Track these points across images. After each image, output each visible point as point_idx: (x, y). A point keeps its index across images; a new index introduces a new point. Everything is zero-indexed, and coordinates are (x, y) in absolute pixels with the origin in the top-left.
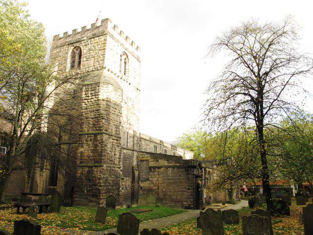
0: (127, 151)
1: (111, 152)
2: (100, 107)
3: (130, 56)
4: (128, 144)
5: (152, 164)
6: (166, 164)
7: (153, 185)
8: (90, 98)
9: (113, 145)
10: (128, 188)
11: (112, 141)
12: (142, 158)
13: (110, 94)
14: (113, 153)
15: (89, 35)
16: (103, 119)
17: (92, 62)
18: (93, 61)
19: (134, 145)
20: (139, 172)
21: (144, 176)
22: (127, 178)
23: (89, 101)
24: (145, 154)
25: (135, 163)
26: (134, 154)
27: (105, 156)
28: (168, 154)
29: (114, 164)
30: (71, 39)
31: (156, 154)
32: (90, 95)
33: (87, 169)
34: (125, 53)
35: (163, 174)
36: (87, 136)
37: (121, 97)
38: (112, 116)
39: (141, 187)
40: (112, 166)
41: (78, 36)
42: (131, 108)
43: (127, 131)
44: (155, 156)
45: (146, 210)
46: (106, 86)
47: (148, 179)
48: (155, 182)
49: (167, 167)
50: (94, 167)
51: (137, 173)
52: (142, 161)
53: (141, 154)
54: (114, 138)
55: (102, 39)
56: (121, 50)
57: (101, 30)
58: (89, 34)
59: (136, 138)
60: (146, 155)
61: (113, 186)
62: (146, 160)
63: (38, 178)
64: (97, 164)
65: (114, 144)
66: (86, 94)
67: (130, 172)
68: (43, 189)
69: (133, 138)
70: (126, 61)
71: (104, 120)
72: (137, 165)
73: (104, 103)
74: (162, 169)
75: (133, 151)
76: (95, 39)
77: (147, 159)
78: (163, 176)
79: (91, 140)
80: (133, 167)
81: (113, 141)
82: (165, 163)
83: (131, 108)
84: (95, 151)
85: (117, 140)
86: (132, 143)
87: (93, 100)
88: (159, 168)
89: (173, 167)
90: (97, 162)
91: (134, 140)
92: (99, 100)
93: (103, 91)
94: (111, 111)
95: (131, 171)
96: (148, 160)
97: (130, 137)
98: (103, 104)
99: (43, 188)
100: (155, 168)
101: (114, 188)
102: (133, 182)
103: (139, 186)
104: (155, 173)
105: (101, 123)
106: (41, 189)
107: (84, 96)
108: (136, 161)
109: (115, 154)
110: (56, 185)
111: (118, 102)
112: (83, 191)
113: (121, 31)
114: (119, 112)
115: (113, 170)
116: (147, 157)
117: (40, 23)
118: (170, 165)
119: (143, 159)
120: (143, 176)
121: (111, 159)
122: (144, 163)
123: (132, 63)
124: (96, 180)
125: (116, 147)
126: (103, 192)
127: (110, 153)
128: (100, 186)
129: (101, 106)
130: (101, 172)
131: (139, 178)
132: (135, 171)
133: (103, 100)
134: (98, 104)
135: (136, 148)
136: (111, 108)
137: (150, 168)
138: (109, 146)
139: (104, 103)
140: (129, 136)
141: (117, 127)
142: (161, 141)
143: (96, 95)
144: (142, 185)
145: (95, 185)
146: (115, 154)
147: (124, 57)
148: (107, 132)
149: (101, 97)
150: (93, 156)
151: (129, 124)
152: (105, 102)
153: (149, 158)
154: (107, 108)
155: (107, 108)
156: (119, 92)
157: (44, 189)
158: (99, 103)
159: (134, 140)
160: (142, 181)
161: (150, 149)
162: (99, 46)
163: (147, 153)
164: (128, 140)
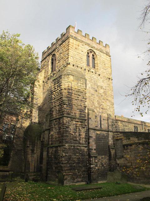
0: (101, 132)
1: (75, 133)
2: (62, 95)
3: (97, 52)
4: (102, 126)
5: (125, 142)
6: (137, 141)
7: (127, 162)
8: (57, 89)
9: (76, 126)
10: (105, 165)
11: (74, 123)
12: (117, 137)
13: (71, 83)
14: (77, 134)
15: (60, 43)
16: (64, 105)
17: (61, 62)
18: (62, 62)
19: (108, 126)
20: (115, 151)
21: (120, 154)
22: (103, 156)
23: (56, 92)
24: (119, 133)
25: (111, 142)
26: (109, 134)
27: (67, 136)
28: (139, 131)
29: (80, 143)
30: (50, 51)
31: (137, 132)
32: (56, 87)
33: (54, 149)
34: (91, 51)
35: (135, 151)
36: (55, 121)
37: (84, 85)
38: (74, 102)
39: (118, 164)
40: (76, 145)
41: (54, 47)
42: (103, 95)
43: (100, 114)
44: (128, 135)
45: (93, 188)
46: (67, 77)
47: (123, 157)
48: (128, 159)
49: (136, 144)
50: (58, 147)
51: (113, 152)
52: (117, 140)
53: (116, 134)
54: (77, 120)
55: (67, 43)
56: (86, 48)
57: (66, 36)
58: (60, 42)
59: (110, 120)
60: (120, 135)
61: (79, 163)
62: (120, 139)
63: (30, 158)
64: (60, 144)
65: (78, 125)
66: (54, 88)
67: (104, 149)
68: (34, 168)
69: (108, 120)
70: (94, 57)
71: (65, 106)
72: (114, 144)
73: (66, 91)
74: (133, 146)
75: (108, 131)
76: (63, 44)
77: (121, 138)
78: (135, 153)
79: (57, 124)
80: (109, 146)
81: (77, 123)
82: (136, 140)
83: (103, 95)
84: (59, 133)
85: (81, 122)
86: (107, 125)
87: (58, 91)
88: (131, 145)
89: (143, 144)
90: (60, 142)
91: (108, 122)
92: (61, 90)
93: (65, 81)
94: (73, 97)
95: (107, 149)
96: (122, 139)
97: (104, 119)
98: (65, 93)
99: (35, 166)
100: (127, 145)
101: (80, 165)
102: (110, 159)
103: (116, 163)
104: (128, 151)
105: (63, 108)
106: (33, 167)
107: (53, 89)
108: (112, 141)
109: (80, 135)
110: (42, 164)
111: (81, 90)
112: (53, 168)
113: (106, 44)
114: (83, 98)
115: (78, 149)
116: (121, 136)
117: (29, 46)
118: (140, 141)
119: (118, 138)
120: (119, 154)
121: (75, 139)
122: (120, 141)
123: (101, 58)
124: (60, 158)
125: (80, 128)
126: (66, 169)
127: (73, 134)
128: (62, 164)
129: (64, 94)
130: (63, 151)
131: (116, 156)
132: (111, 150)
133: (65, 89)
134: (61, 93)
135: (110, 129)
136: (73, 95)
137: (124, 146)
138: (72, 127)
139: (66, 91)
140: (102, 119)
141: (82, 111)
142: (142, 122)
143: (60, 86)
144: (118, 162)
145: (59, 163)
146: (80, 135)
147: (91, 55)
148: (69, 116)
149: (63, 87)
150: (59, 137)
151: (102, 108)
152: (67, 90)
153: (122, 137)
154: (68, 95)
155: (68, 95)
156: (82, 81)
157: (36, 167)
158: (62, 92)
159: (108, 122)
160: (119, 159)
161: (130, 128)
162: (65, 48)
163: (121, 132)
164: (102, 123)
